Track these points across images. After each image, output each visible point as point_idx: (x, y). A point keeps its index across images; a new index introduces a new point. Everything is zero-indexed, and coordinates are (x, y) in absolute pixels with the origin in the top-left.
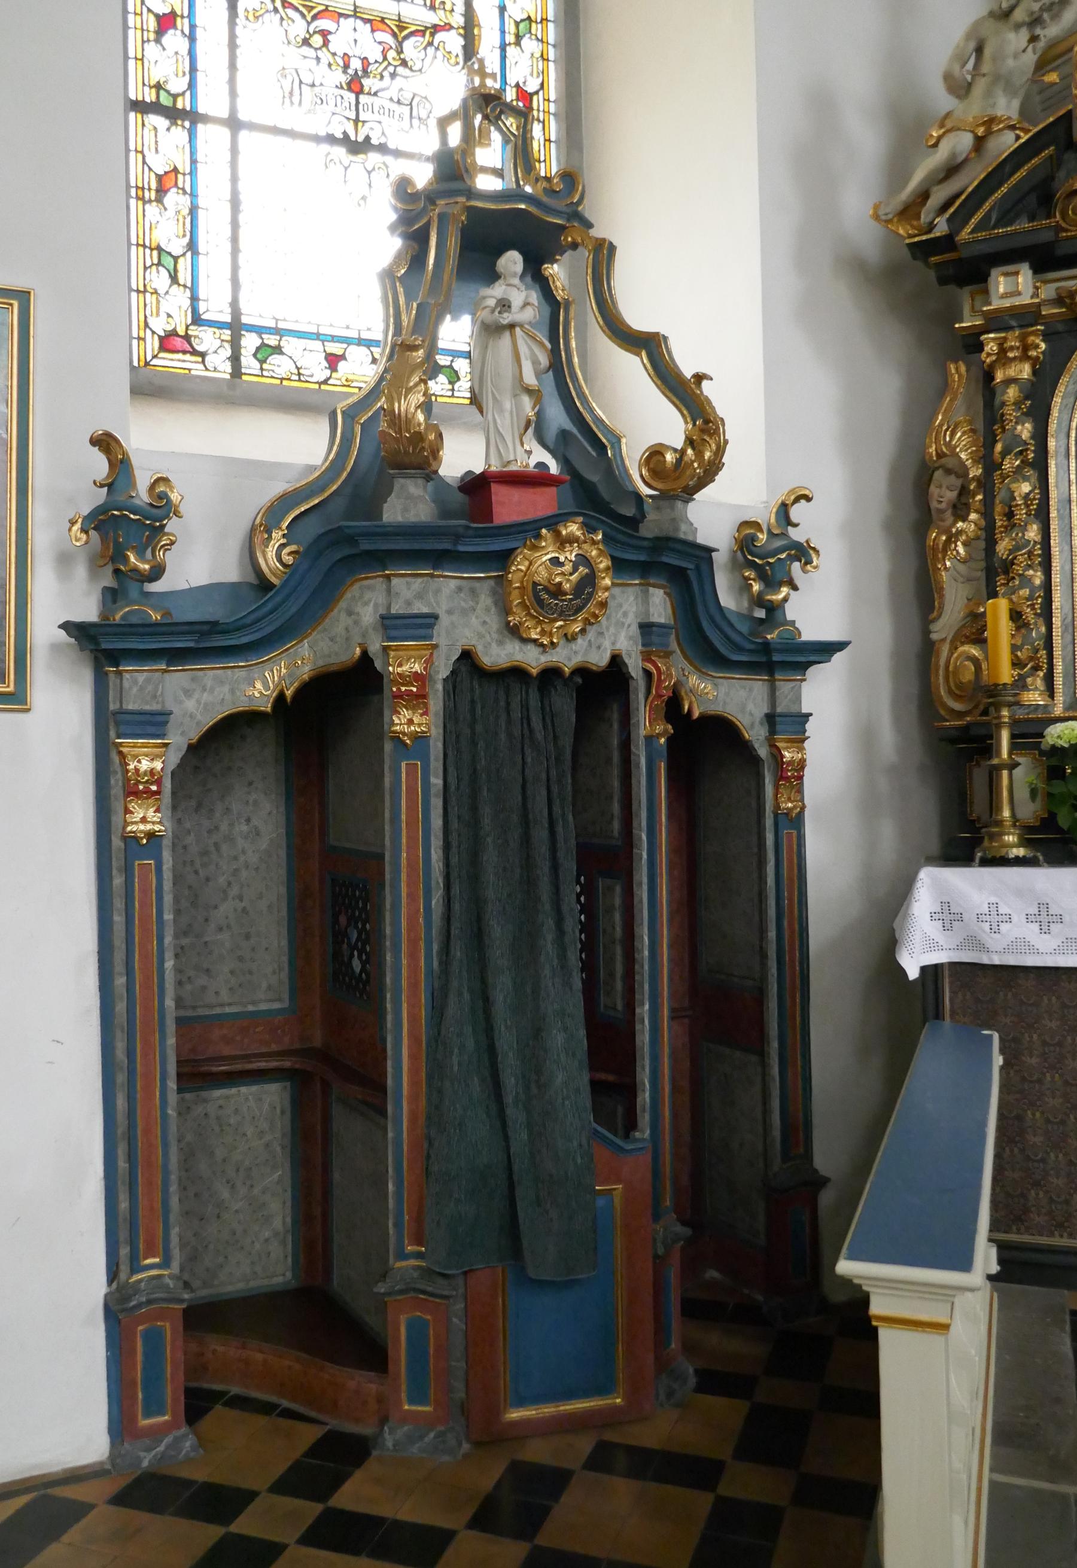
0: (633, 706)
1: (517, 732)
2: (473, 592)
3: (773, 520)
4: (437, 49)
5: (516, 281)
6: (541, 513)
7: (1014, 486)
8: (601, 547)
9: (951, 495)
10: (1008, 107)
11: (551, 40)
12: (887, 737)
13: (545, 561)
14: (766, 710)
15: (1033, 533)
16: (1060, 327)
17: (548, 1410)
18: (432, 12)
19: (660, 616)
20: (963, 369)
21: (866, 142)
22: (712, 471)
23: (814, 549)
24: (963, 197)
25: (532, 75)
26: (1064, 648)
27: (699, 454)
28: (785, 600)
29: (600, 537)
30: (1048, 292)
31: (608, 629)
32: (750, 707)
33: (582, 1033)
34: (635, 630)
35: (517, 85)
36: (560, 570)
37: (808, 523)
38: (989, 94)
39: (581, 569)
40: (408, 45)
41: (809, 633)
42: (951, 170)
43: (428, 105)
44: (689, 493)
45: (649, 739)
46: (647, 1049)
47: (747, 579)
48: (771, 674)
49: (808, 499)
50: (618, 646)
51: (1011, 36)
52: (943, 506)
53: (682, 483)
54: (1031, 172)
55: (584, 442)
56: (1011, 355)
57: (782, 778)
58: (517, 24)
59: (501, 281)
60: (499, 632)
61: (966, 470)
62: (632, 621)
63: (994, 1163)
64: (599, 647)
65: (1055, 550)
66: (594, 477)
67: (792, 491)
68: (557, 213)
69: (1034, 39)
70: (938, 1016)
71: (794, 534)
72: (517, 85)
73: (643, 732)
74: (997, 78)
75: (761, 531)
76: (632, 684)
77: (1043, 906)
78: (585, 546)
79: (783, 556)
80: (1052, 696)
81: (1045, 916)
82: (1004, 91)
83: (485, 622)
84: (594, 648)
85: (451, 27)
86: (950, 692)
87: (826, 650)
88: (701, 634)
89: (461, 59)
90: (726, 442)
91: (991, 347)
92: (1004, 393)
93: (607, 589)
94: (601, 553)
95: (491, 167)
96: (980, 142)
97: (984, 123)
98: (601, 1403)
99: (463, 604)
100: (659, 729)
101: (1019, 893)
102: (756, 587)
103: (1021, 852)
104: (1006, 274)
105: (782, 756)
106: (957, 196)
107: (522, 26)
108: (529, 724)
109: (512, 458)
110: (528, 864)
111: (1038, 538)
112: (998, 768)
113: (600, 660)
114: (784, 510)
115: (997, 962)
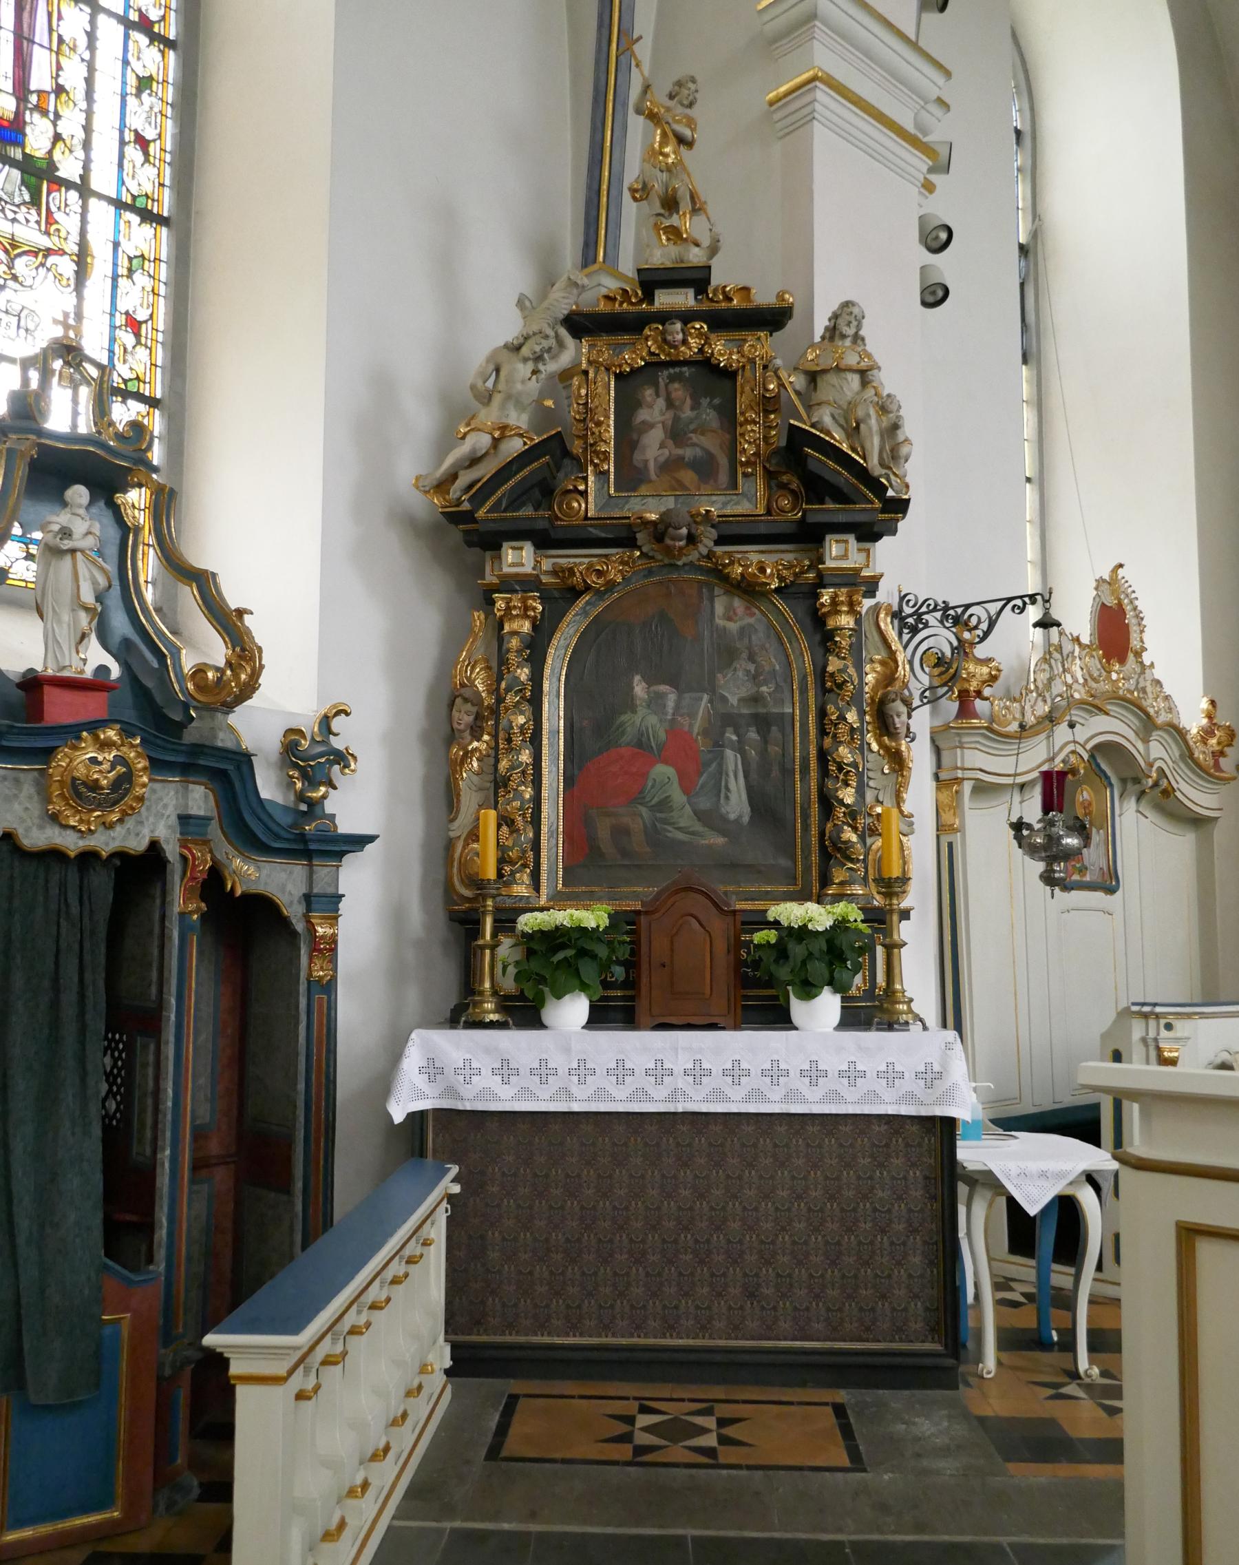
0: (168, 886)
1: (53, 907)
2: (17, 781)
3: (316, 729)
4: (48, 270)
5: (82, 511)
6: (82, 719)
7: (512, 717)
8: (139, 750)
9: (469, 719)
10: (518, 419)
11: (163, 278)
12: (416, 916)
13: (88, 759)
14: (304, 890)
15: (525, 757)
16: (556, 594)
17: (45, 1529)
18: (45, 237)
19: (199, 808)
20: (482, 617)
21: (418, 420)
22: (249, 689)
23: (352, 755)
24: (480, 484)
25: (142, 305)
26: (549, 850)
27: (236, 676)
28: (324, 797)
29: (138, 741)
30: (547, 565)
31: (147, 818)
32: (290, 887)
33: (98, 1178)
34: (174, 820)
35: (127, 313)
36: (97, 768)
37: (346, 735)
38: (503, 407)
39: (119, 768)
40: (20, 264)
41: (345, 826)
42: (474, 461)
43: (36, 318)
44: (229, 707)
45: (182, 915)
46: (166, 1190)
47: (292, 777)
48: (310, 859)
49: (347, 714)
50: (156, 834)
51: (520, 366)
52: (462, 727)
53: (222, 697)
54: (531, 473)
55: (143, 652)
56: (514, 612)
57: (315, 950)
58: (130, 259)
59: (68, 510)
60: (40, 817)
61: (482, 700)
62: (171, 813)
63: (447, 1276)
64: (137, 835)
65: (545, 771)
66: (149, 683)
67: (334, 706)
68: (124, 458)
69: (535, 372)
70: (422, 1154)
71: (337, 743)
72: (127, 313)
73: (176, 909)
74: (509, 397)
75: (304, 738)
76: (169, 867)
77: (505, 1062)
78: (124, 749)
79: (323, 760)
80: (537, 888)
81: (506, 1070)
82: (515, 406)
83: (27, 809)
84: (132, 835)
85: (64, 253)
86: (462, 881)
87: (360, 841)
88: (244, 820)
89: (72, 282)
90: (262, 667)
91: (500, 604)
92: (509, 642)
93: (144, 785)
94: (139, 755)
95: (66, 414)
96: (496, 442)
97: (499, 428)
98: (99, 1517)
99: (7, 791)
100: (191, 907)
101: (487, 1051)
102: (299, 785)
103: (494, 1017)
104: (513, 548)
105: (316, 931)
106: (479, 480)
107: (135, 262)
108: (66, 900)
109: (67, 663)
110: (55, 1023)
111: (529, 761)
112: (483, 948)
113: (138, 845)
114: (326, 721)
115: (469, 1108)
